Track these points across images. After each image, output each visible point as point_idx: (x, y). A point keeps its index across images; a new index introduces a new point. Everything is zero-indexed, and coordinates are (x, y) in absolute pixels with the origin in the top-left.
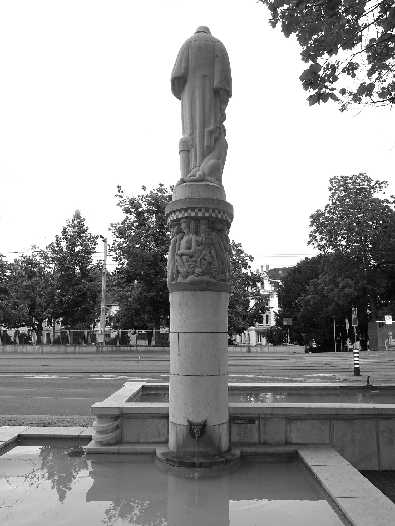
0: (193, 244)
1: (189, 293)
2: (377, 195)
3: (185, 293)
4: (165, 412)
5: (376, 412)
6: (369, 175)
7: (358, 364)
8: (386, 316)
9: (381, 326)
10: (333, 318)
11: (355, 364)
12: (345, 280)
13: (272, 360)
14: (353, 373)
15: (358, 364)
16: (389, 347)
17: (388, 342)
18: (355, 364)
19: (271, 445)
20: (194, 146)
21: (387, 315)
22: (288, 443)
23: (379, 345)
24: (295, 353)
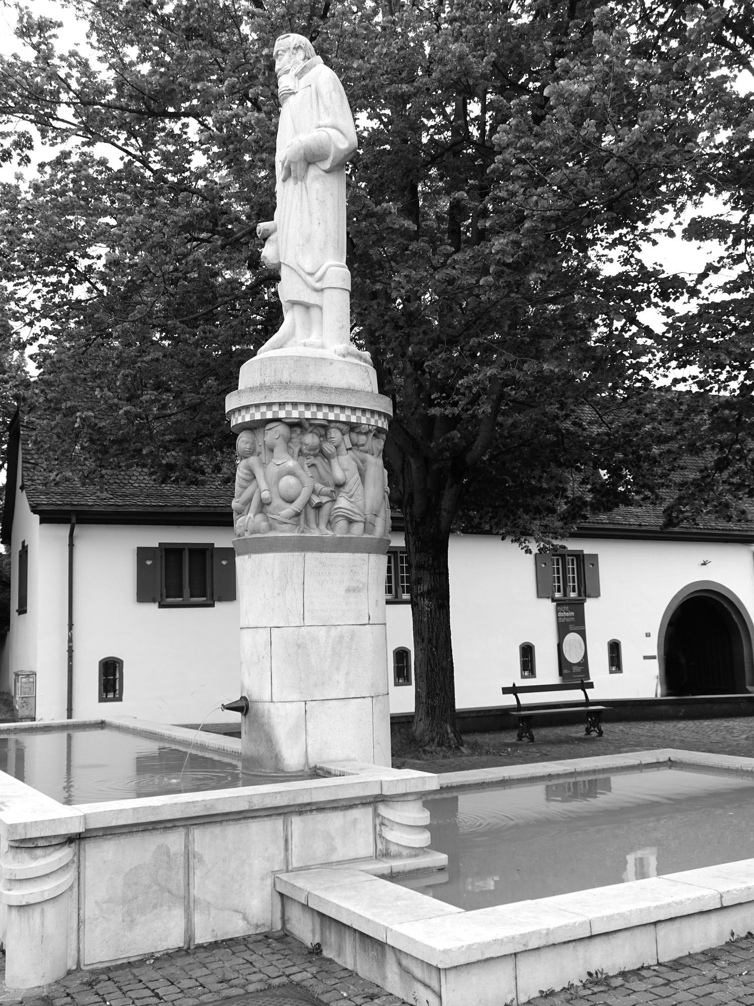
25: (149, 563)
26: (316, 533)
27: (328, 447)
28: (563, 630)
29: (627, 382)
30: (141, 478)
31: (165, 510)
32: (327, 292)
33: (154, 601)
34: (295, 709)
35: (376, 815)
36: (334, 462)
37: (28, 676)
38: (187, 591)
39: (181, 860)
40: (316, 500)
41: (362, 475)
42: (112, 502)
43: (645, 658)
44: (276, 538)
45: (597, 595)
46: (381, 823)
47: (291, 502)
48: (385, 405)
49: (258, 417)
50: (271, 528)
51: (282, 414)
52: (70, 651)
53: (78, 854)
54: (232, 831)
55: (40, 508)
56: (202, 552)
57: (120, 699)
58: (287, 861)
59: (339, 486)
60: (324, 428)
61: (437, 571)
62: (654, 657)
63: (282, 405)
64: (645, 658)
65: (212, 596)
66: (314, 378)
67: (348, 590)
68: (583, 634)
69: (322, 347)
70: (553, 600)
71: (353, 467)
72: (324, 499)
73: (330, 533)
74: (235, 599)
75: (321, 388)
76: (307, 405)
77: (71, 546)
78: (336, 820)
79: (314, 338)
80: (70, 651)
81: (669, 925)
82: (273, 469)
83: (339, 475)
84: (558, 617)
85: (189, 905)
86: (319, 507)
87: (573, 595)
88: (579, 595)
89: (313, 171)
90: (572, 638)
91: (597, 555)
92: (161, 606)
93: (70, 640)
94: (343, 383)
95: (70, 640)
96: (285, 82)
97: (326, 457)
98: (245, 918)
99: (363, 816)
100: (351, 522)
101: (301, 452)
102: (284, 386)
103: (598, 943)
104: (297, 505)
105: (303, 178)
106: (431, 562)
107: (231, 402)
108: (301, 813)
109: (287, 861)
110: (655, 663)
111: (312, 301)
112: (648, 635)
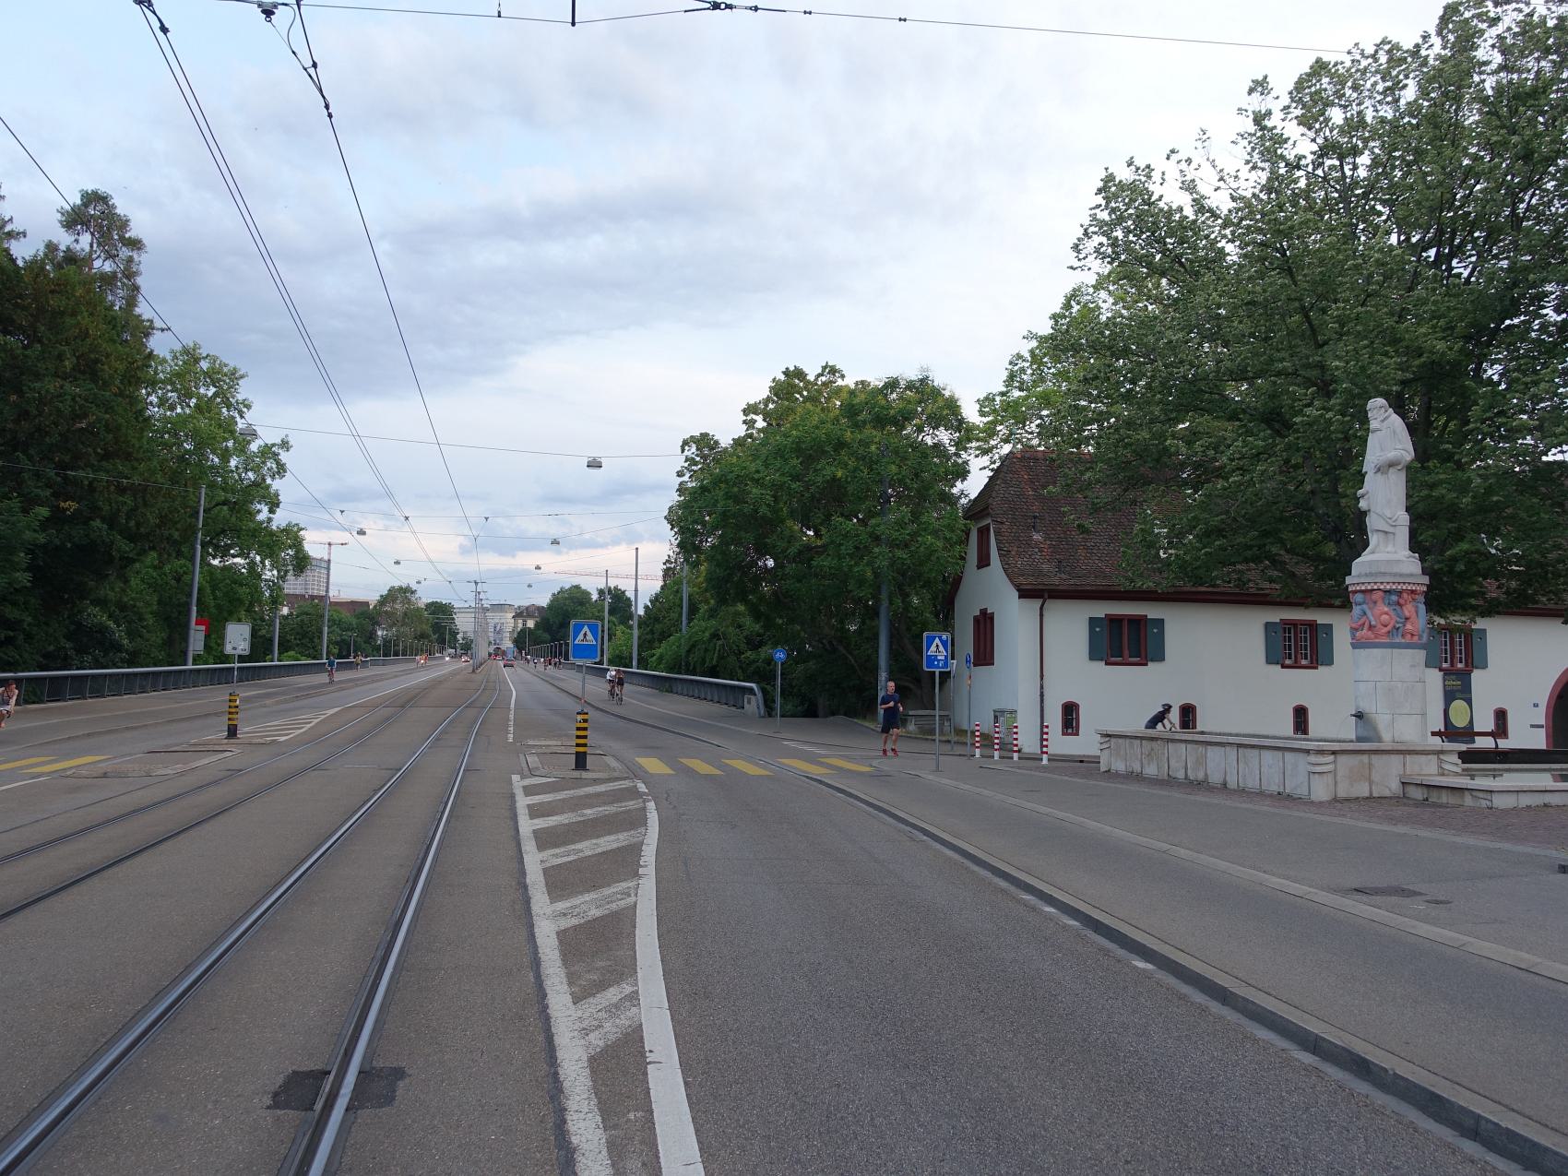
27: (1402, 601)
28: (1449, 697)
30: (1086, 561)
31: (1112, 589)
32: (1398, 527)
34: (1388, 717)
35: (1439, 758)
36: (1404, 608)
37: (1011, 713)
38: (1126, 652)
39: (1367, 766)
40: (1397, 626)
41: (1417, 612)
42: (1072, 582)
43: (1532, 726)
44: (1379, 642)
45: (1484, 666)
46: (1441, 761)
47: (1386, 626)
48: (1426, 580)
49: (1369, 588)
50: (1376, 638)
51: (1382, 587)
52: (1042, 695)
53: (1335, 758)
54: (1385, 757)
55: (1021, 587)
56: (1138, 622)
57: (1077, 734)
59: (1407, 619)
60: (1400, 593)
62: (1542, 726)
63: (1382, 583)
64: (1532, 726)
65: (1146, 658)
66: (1396, 570)
67: (1412, 666)
68: (1469, 702)
69: (1395, 552)
70: (1441, 670)
71: (1413, 609)
72: (1400, 625)
73: (1403, 641)
74: (1164, 660)
75: (1401, 575)
76: (1394, 583)
77: (1041, 615)
78: (1423, 758)
79: (1390, 548)
80: (1042, 695)
82: (1377, 611)
83: (1407, 614)
84: (1445, 685)
85: (1371, 783)
86: (1398, 628)
87: (1460, 666)
88: (1467, 665)
89: (1391, 470)
90: (1459, 705)
91: (1485, 630)
92: (1107, 664)
93: (1042, 687)
94: (1408, 572)
95: (1042, 687)
96: (1373, 424)
97: (1401, 605)
98: (1390, 790)
99: (1434, 758)
100: (1412, 635)
101: (1389, 604)
102: (1384, 574)
103: (1547, 794)
104: (1389, 628)
105: (1386, 473)
107: (1348, 580)
108: (1409, 754)
110: (1542, 732)
111: (1390, 531)
112: (1536, 705)
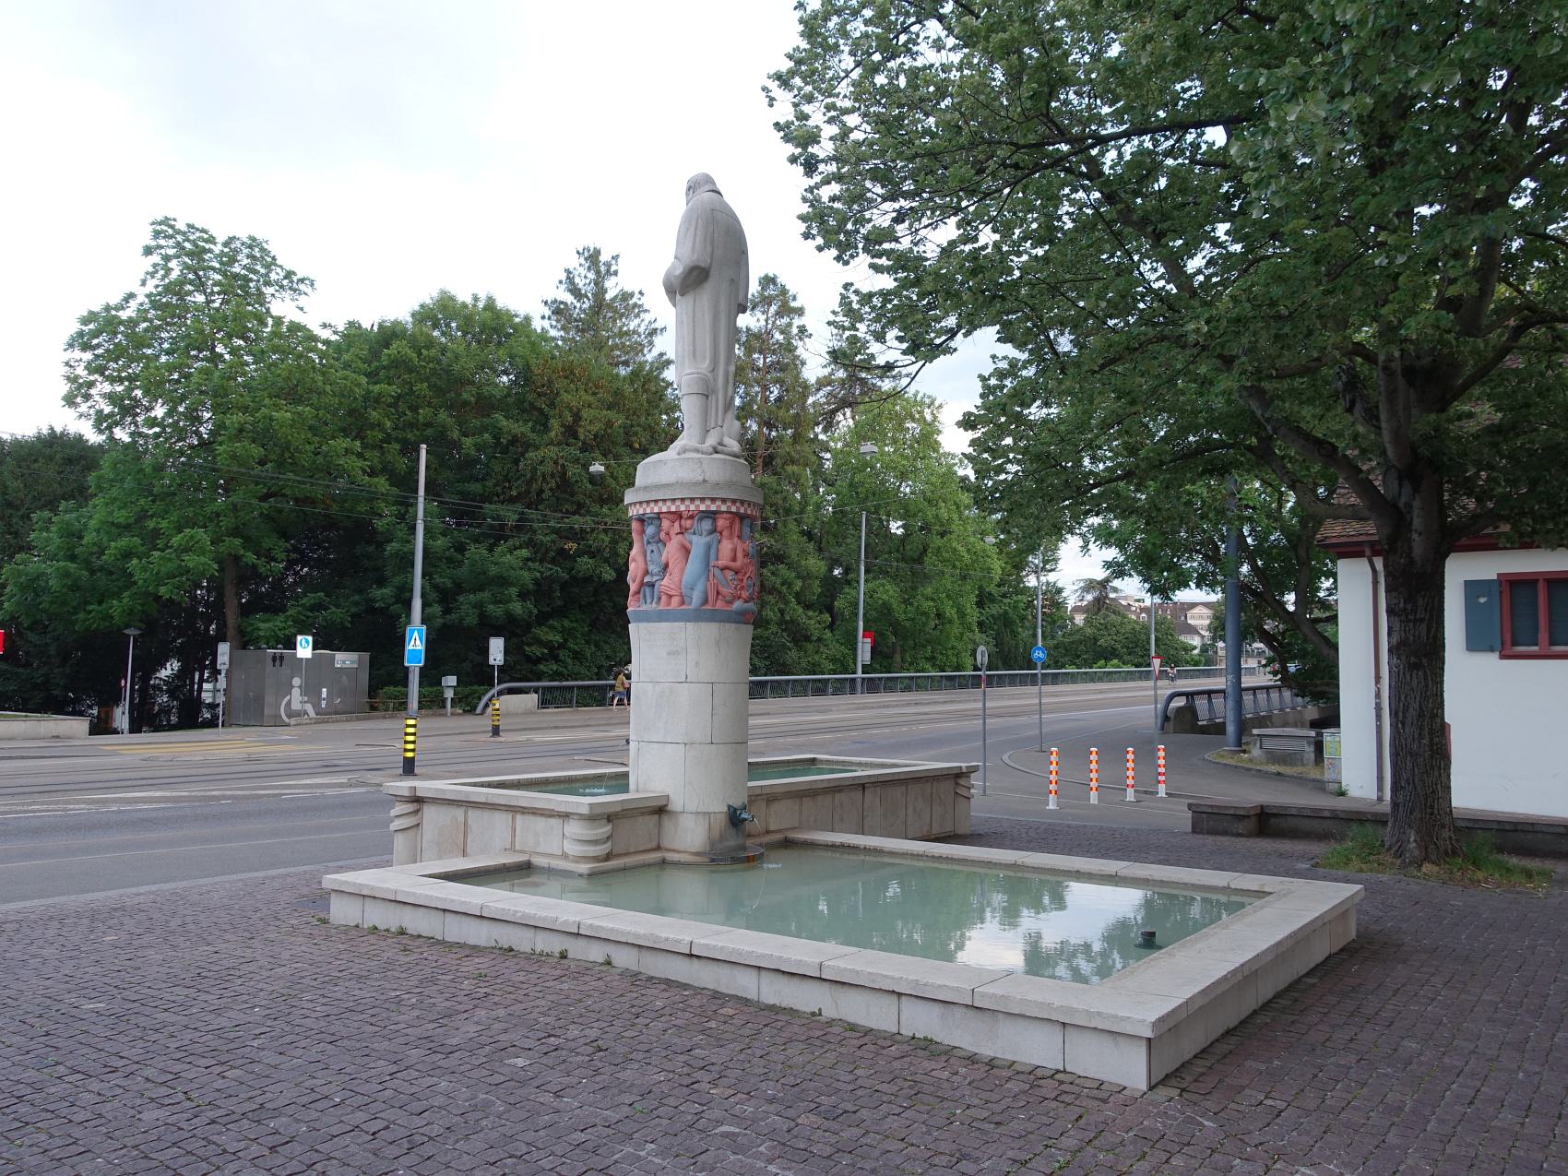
0: (740, 555)
1: (733, 626)
2: (282, 307)
3: (727, 625)
4: (663, 803)
5: (832, 784)
6: (273, 248)
7: (413, 750)
8: (299, 638)
9: (278, 663)
10: (129, 636)
11: (406, 750)
12: (188, 530)
13: (23, 758)
14: (401, 771)
15: (413, 750)
16: (289, 716)
17: (289, 703)
18: (406, 750)
19: (678, 852)
20: (714, 391)
21: (301, 634)
22: (768, 832)
23: (267, 711)
24: (58, 737)
25: (1482, 600)
26: (644, 607)
29: (909, 425)
33: (1492, 650)
38: (1543, 636)
58: (513, 843)
61: (1412, 617)
81: (453, 915)
86: (652, 585)
94: (672, 479)
106: (1402, 605)
109: (513, 843)
